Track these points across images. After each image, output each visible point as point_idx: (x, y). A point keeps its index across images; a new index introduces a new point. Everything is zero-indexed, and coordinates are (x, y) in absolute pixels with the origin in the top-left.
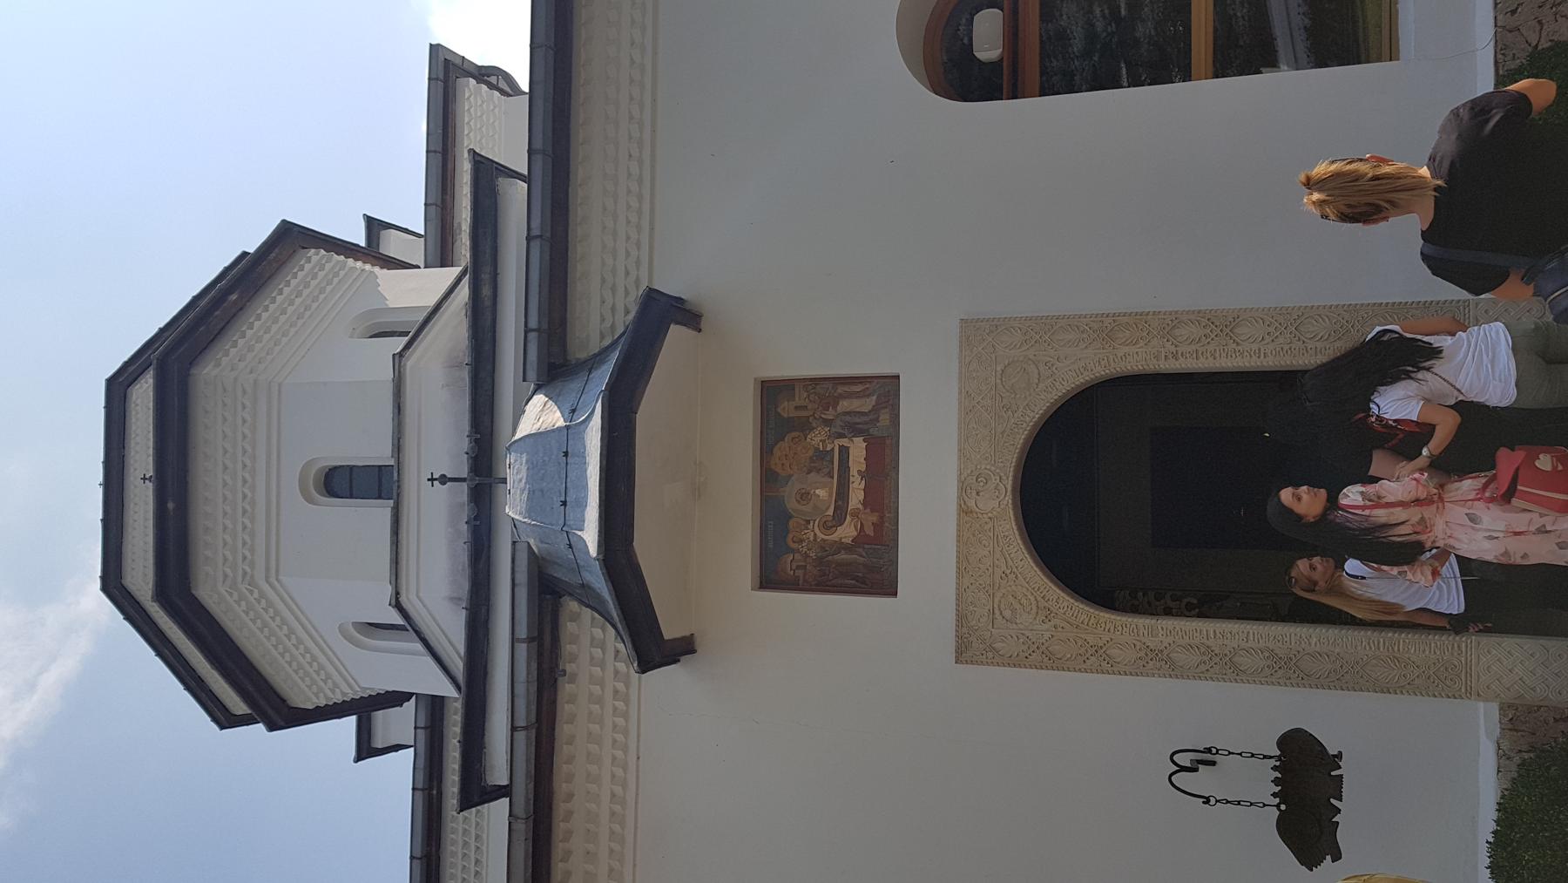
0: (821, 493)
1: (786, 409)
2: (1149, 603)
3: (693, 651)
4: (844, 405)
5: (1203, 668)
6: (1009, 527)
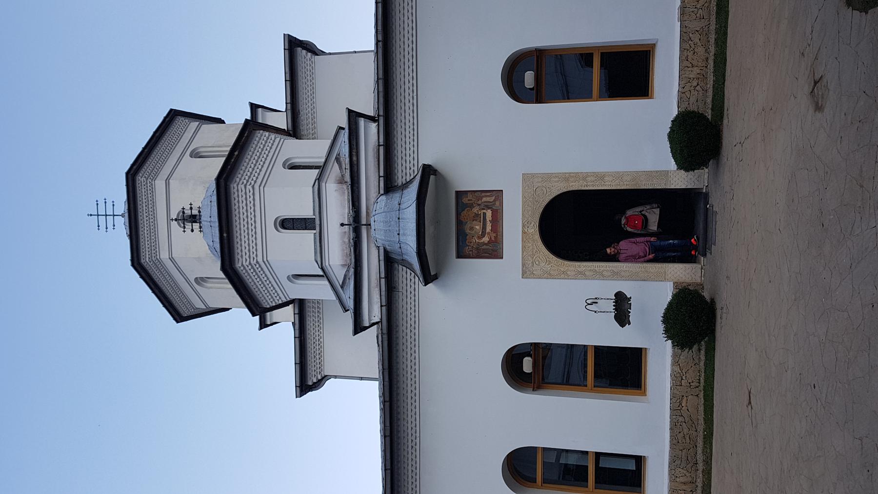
1: (465, 200)
4: (484, 199)
6: (537, 236)
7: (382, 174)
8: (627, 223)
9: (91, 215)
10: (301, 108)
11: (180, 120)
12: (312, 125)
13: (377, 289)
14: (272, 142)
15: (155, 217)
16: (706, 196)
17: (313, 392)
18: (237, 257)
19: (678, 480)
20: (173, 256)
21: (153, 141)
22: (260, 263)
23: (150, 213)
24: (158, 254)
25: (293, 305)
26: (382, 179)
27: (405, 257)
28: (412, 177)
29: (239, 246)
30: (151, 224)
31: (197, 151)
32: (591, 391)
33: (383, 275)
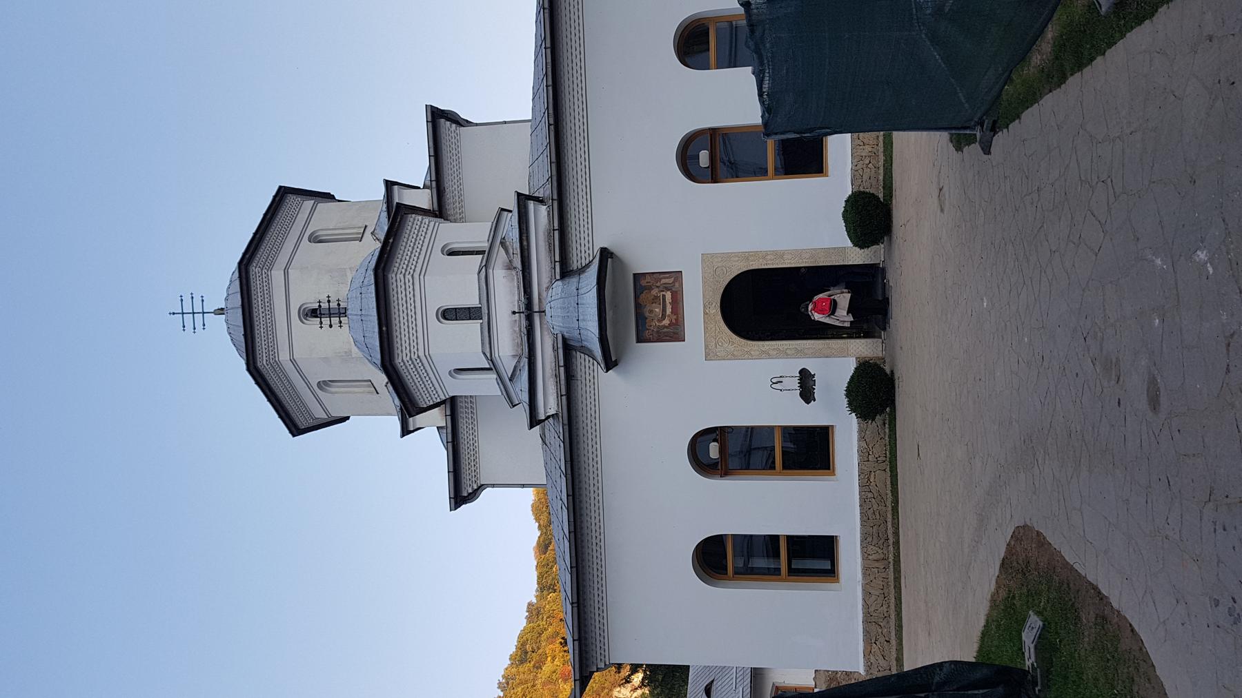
0: (657, 310)
1: (643, 283)
4: (663, 281)
6: (719, 317)
7: (557, 259)
8: (813, 309)
9: (174, 314)
10: (446, 185)
11: (291, 199)
12: (459, 203)
13: (552, 379)
14: (426, 226)
15: (272, 313)
16: (883, 270)
18: (397, 351)
19: (870, 557)
21: (263, 227)
22: (421, 357)
23: (267, 309)
24: (276, 355)
26: (557, 264)
27: (585, 343)
28: (587, 261)
29: (398, 340)
30: (268, 321)
31: (317, 234)
32: (780, 474)
33: (562, 363)
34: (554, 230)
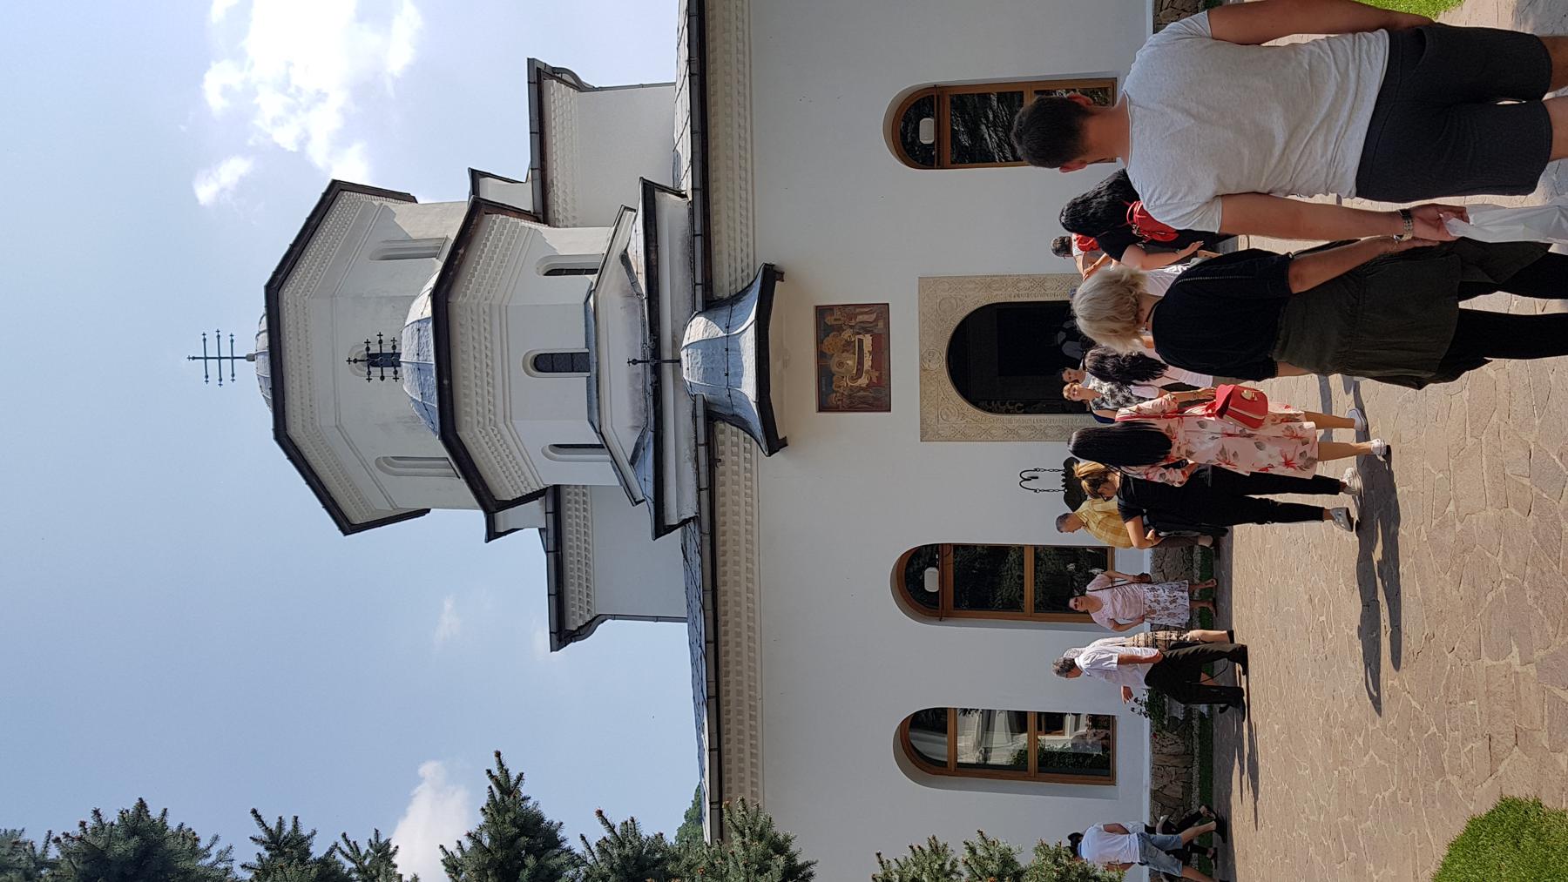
0: (850, 362)
2: (998, 408)
3: (786, 445)
4: (860, 318)
5: (1032, 436)
6: (945, 376)
7: (699, 280)
9: (194, 358)
17: (577, 642)
19: (1165, 750)
20: (342, 422)
25: (544, 497)
26: (699, 288)
27: (737, 411)
28: (746, 285)
34: (694, 236)
